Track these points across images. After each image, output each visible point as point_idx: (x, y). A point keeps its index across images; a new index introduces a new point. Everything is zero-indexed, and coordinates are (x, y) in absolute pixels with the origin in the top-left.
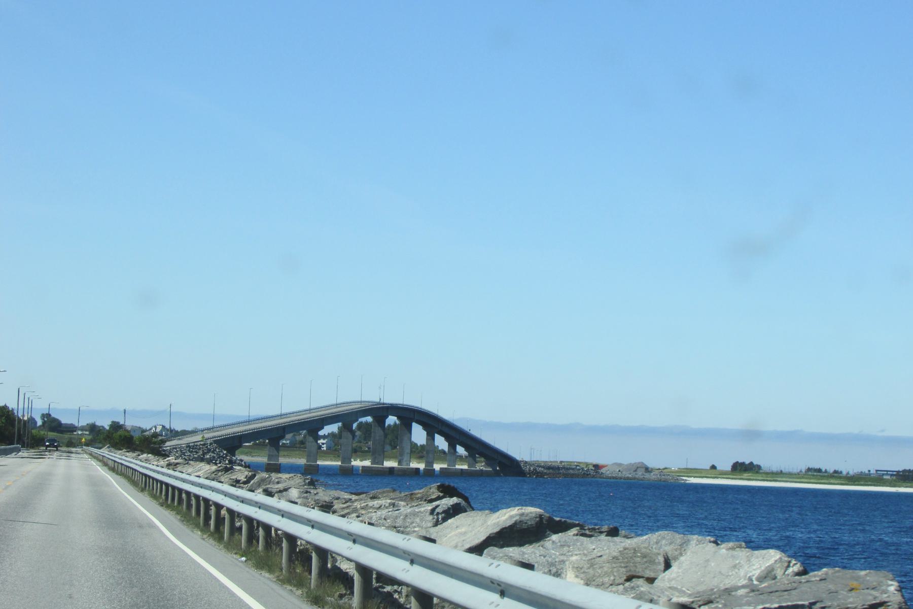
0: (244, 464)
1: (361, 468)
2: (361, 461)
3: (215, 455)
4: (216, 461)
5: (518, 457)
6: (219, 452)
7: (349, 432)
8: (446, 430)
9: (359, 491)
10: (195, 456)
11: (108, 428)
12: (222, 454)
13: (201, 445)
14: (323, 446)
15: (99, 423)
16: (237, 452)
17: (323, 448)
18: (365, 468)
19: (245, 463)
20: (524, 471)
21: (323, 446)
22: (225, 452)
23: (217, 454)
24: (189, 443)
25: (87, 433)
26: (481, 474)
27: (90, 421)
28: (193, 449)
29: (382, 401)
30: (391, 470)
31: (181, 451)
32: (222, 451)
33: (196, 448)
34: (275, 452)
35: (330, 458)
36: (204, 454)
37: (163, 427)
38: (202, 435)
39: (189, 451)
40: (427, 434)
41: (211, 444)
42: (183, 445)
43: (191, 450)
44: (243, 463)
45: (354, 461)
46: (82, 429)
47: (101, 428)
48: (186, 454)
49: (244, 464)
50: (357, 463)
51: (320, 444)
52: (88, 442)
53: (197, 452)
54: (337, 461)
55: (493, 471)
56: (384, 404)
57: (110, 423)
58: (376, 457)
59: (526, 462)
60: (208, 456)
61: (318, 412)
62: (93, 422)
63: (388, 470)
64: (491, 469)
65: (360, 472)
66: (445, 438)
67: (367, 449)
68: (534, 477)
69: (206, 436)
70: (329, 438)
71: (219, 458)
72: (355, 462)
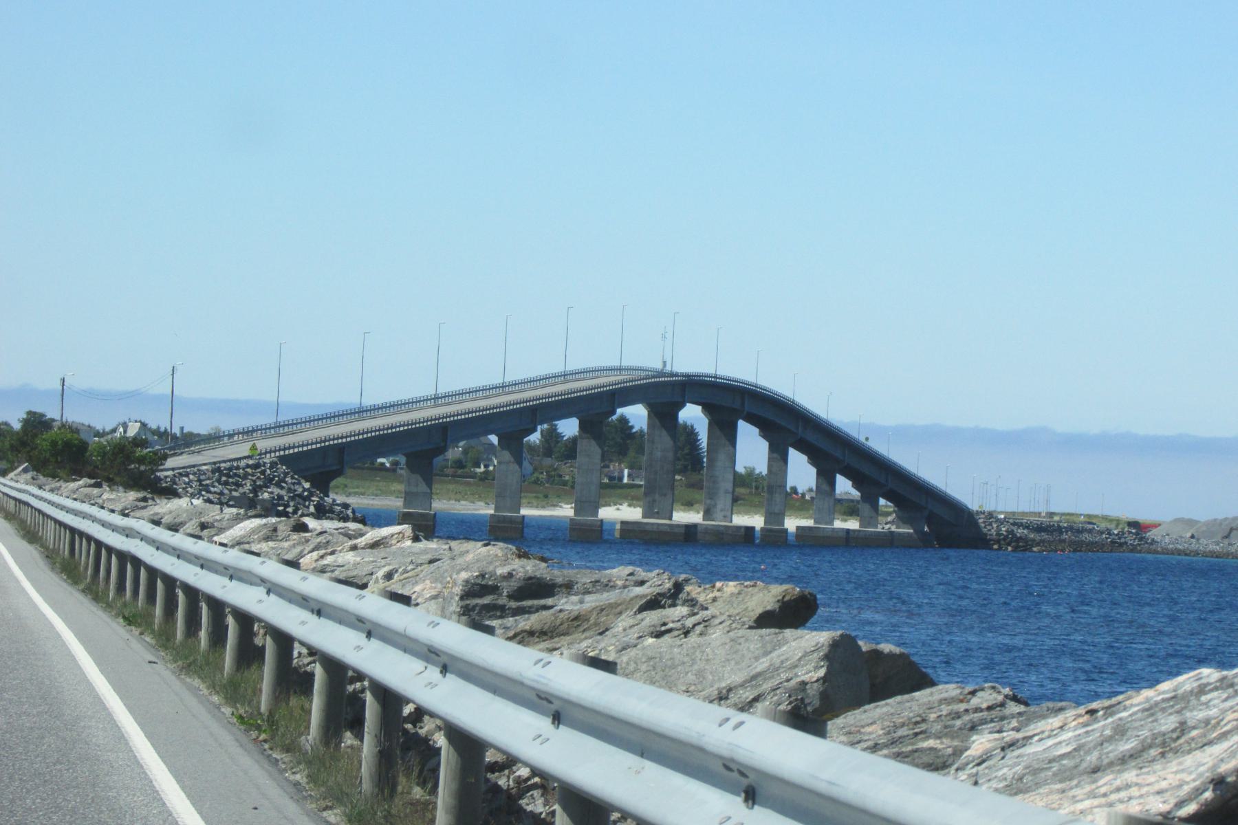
0: (351, 515)
3: (283, 492)
4: (287, 506)
5: (973, 504)
7: (594, 439)
8: (811, 437)
10: (234, 494)
12: (300, 490)
13: (248, 466)
18: (629, 529)
19: (354, 512)
20: (986, 535)
22: (307, 485)
23: (289, 490)
24: (220, 462)
26: (889, 542)
29: (668, 368)
31: (200, 481)
32: (299, 483)
34: (423, 487)
36: (256, 490)
37: (144, 425)
38: (249, 445)
39: (219, 481)
41: (273, 465)
42: (204, 468)
43: (224, 479)
44: (349, 512)
48: (212, 489)
49: (351, 515)
53: (238, 485)
55: (915, 536)
56: (672, 375)
58: (654, 501)
59: (991, 515)
60: (266, 496)
63: (683, 530)
64: (912, 531)
66: (809, 458)
68: (1010, 548)
69: (262, 445)
71: (292, 498)
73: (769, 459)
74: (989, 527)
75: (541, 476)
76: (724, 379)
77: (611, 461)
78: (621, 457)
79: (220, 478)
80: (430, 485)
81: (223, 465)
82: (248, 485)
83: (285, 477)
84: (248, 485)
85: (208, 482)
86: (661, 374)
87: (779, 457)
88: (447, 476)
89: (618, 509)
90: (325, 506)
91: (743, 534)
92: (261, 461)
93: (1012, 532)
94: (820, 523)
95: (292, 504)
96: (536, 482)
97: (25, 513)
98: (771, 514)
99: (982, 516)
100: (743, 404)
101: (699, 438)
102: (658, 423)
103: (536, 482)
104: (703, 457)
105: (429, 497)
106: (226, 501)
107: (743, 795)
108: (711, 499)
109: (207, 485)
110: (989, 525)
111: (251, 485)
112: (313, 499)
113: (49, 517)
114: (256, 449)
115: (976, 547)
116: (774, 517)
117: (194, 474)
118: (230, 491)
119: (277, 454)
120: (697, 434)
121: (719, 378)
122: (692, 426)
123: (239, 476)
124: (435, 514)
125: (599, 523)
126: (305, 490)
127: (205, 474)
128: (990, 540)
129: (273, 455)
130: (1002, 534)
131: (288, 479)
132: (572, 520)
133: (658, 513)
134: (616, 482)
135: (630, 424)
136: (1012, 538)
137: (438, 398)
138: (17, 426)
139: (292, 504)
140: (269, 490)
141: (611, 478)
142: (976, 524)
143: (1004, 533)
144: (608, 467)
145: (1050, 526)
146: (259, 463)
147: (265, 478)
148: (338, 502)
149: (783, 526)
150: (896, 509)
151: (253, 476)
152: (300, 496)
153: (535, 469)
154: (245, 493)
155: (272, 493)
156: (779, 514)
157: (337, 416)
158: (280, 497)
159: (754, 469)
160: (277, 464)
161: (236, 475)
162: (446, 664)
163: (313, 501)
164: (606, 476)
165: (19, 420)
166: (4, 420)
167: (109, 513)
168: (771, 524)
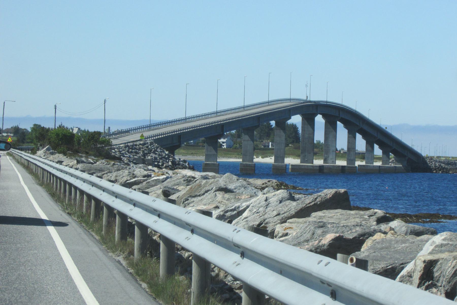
0: (187, 166)
1: (290, 167)
2: (263, 158)
3: (157, 156)
4: (159, 162)
5: (424, 154)
6: (161, 152)
7: (282, 129)
8: (366, 128)
9: (305, 194)
10: (135, 157)
11: (30, 130)
12: (164, 155)
13: (140, 144)
14: (223, 144)
15: (22, 127)
16: (176, 151)
17: (224, 146)
18: (294, 167)
19: (189, 164)
20: (430, 167)
21: (223, 144)
22: (167, 153)
23: (159, 155)
24: (128, 143)
25: (12, 135)
26: (394, 171)
27: (14, 125)
28: (132, 149)
29: (309, 99)
30: (321, 168)
31: (120, 152)
32: (164, 152)
33: (135, 149)
34: (214, 152)
35: (234, 156)
36: (145, 155)
37: (79, 129)
38: (140, 134)
39: (128, 151)
40: (348, 132)
41: (151, 144)
42: (121, 145)
43: (130, 150)
44: (187, 164)
45: (257, 158)
46: (7, 131)
47: (25, 131)
48: (125, 155)
49: (187, 166)
50: (258, 160)
51: (221, 143)
52: (14, 143)
53: (137, 153)
54: (239, 158)
55: (403, 168)
56: (310, 102)
57: (33, 126)
58: (305, 156)
59: (431, 158)
60: (149, 157)
61: (226, 114)
62: (17, 125)
63: (318, 168)
64: (401, 166)
65: (290, 171)
66: (362, 136)
67: (263, 147)
68: (440, 172)
69: (146, 134)
70: (229, 138)
71: (161, 159)
72: (258, 159)
73: (348, 137)
74: (431, 164)
75: (237, 146)
76: (332, 103)
77: (264, 139)
78: (268, 138)
79: (129, 150)
80: (216, 151)
81: (129, 144)
82: (141, 153)
83: (157, 149)
84: (141, 153)
85: (123, 152)
86: (306, 101)
87: (352, 136)
88: (200, 146)
89: (271, 159)
90: (175, 162)
91: (341, 169)
92: (146, 142)
93: (440, 165)
94: (368, 164)
95: (161, 161)
96: (236, 148)
97: (34, 167)
98: (349, 160)
99: (428, 159)
100: (339, 114)
101: (298, 130)
102: (306, 123)
103: (236, 148)
104: (300, 137)
105: (216, 157)
106: (132, 160)
107: (240, 254)
108: (326, 154)
109: (123, 153)
110: (431, 163)
111: (142, 153)
112: (170, 159)
113: (39, 167)
114: (143, 136)
115: (426, 172)
116: (351, 161)
117: (117, 148)
118: (133, 155)
119: (152, 138)
120: (298, 128)
121: (328, 103)
122: (296, 125)
123: (137, 149)
124: (219, 164)
125: (285, 166)
126: (166, 155)
127: (122, 148)
128: (432, 169)
129: (150, 139)
130: (437, 166)
131: (159, 150)
132: (273, 165)
133: (307, 161)
134: (267, 147)
135: (271, 125)
136: (441, 168)
137: (218, 113)
138: (30, 130)
139: (161, 161)
140: (151, 155)
141: (265, 146)
142: (426, 163)
143: (438, 166)
144: (263, 142)
145: (451, 162)
146: (145, 143)
147: (148, 149)
148: (182, 160)
149: (355, 165)
150: (395, 157)
151: (143, 149)
152: (164, 157)
153: (234, 143)
154: (140, 156)
155: (152, 156)
156: (352, 160)
157: (163, 124)
158: (156, 158)
159: (320, 141)
160: (153, 143)
161: (135, 149)
162: (160, 215)
163: (170, 160)
164: (263, 145)
165: (30, 128)
166: (25, 128)
167: (56, 164)
168: (349, 164)
